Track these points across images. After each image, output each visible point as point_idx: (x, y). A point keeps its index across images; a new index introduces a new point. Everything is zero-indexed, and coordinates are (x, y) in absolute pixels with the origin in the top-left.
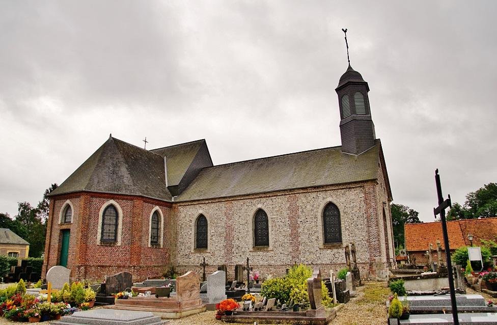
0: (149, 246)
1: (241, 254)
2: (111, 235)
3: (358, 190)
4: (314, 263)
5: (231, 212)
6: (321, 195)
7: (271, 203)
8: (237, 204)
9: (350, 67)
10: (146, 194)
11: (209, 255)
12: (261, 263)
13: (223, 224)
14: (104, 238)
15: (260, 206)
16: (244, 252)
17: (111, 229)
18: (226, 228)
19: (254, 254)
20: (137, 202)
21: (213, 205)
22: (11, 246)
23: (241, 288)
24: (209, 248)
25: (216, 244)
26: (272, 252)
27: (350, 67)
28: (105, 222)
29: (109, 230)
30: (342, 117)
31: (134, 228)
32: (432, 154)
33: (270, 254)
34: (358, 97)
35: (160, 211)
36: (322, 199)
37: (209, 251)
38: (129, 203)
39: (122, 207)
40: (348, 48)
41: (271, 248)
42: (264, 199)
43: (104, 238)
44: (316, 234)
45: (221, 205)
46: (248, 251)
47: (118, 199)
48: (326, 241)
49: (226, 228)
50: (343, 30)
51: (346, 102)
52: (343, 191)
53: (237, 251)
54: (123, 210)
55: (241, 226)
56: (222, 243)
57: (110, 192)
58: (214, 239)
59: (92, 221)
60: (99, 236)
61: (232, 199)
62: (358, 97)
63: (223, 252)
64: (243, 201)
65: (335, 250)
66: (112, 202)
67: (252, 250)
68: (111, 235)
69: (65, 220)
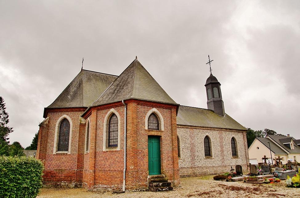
1: (199, 160)
3: (241, 134)
4: (230, 165)
5: (193, 135)
6: (230, 133)
7: (212, 133)
8: (196, 131)
9: (211, 75)
11: (182, 161)
12: (209, 165)
13: (189, 142)
15: (207, 134)
16: (201, 159)
18: (191, 145)
19: (206, 160)
21: (182, 129)
22: (94, 144)
23: (157, 184)
24: (181, 156)
25: (186, 154)
26: (214, 159)
27: (211, 75)
33: (213, 160)
34: (215, 89)
36: (231, 135)
37: (181, 158)
39: (71, 117)
41: (213, 157)
42: (209, 131)
44: (230, 151)
45: (187, 130)
46: (203, 158)
48: (206, 155)
49: (191, 145)
51: (210, 91)
52: (237, 133)
53: (197, 159)
55: (199, 144)
56: (189, 154)
58: (184, 151)
61: (191, 127)
62: (215, 89)
63: (190, 159)
64: (199, 130)
65: (236, 159)
67: (205, 158)
69: (148, 127)
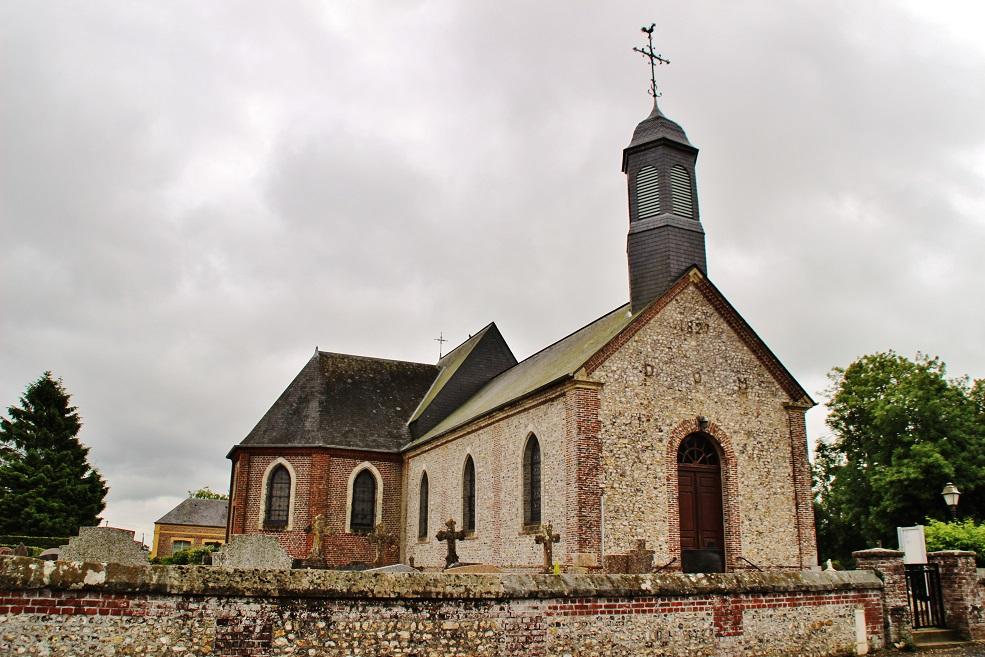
0: (348, 531)
2: (281, 513)
9: (656, 109)
10: (340, 443)
14: (273, 518)
17: (282, 504)
20: (317, 458)
27: (656, 109)
28: (274, 493)
29: (280, 506)
30: (634, 216)
31: (320, 501)
32: (865, 276)
35: (375, 471)
38: (307, 460)
39: (295, 468)
40: (653, 80)
43: (273, 518)
47: (290, 455)
50: (644, 30)
54: (297, 471)
57: (273, 445)
59: (252, 492)
60: (262, 516)
62: (677, 177)
66: (366, 464)
68: (281, 513)
